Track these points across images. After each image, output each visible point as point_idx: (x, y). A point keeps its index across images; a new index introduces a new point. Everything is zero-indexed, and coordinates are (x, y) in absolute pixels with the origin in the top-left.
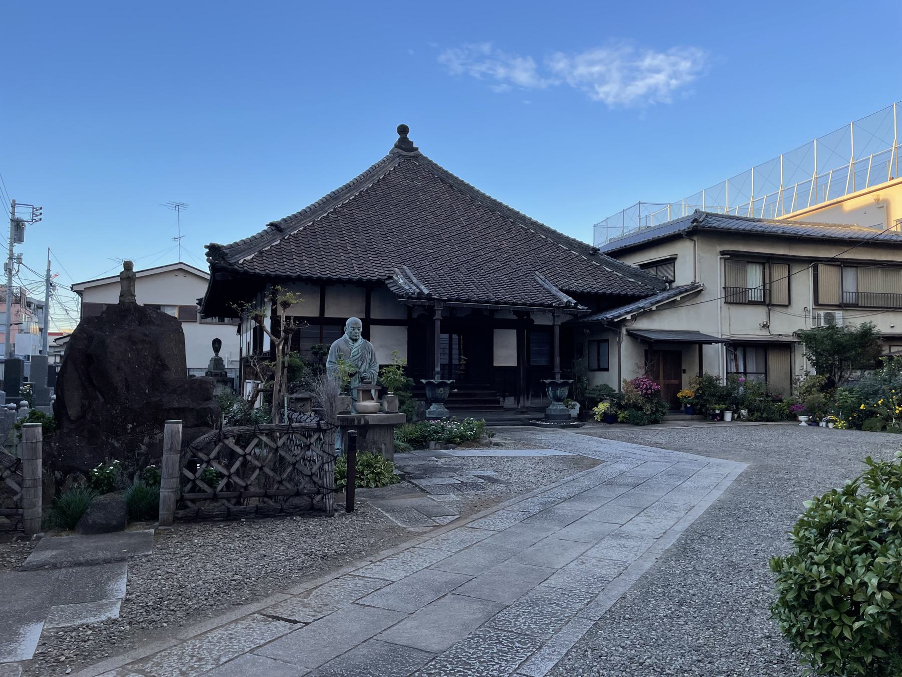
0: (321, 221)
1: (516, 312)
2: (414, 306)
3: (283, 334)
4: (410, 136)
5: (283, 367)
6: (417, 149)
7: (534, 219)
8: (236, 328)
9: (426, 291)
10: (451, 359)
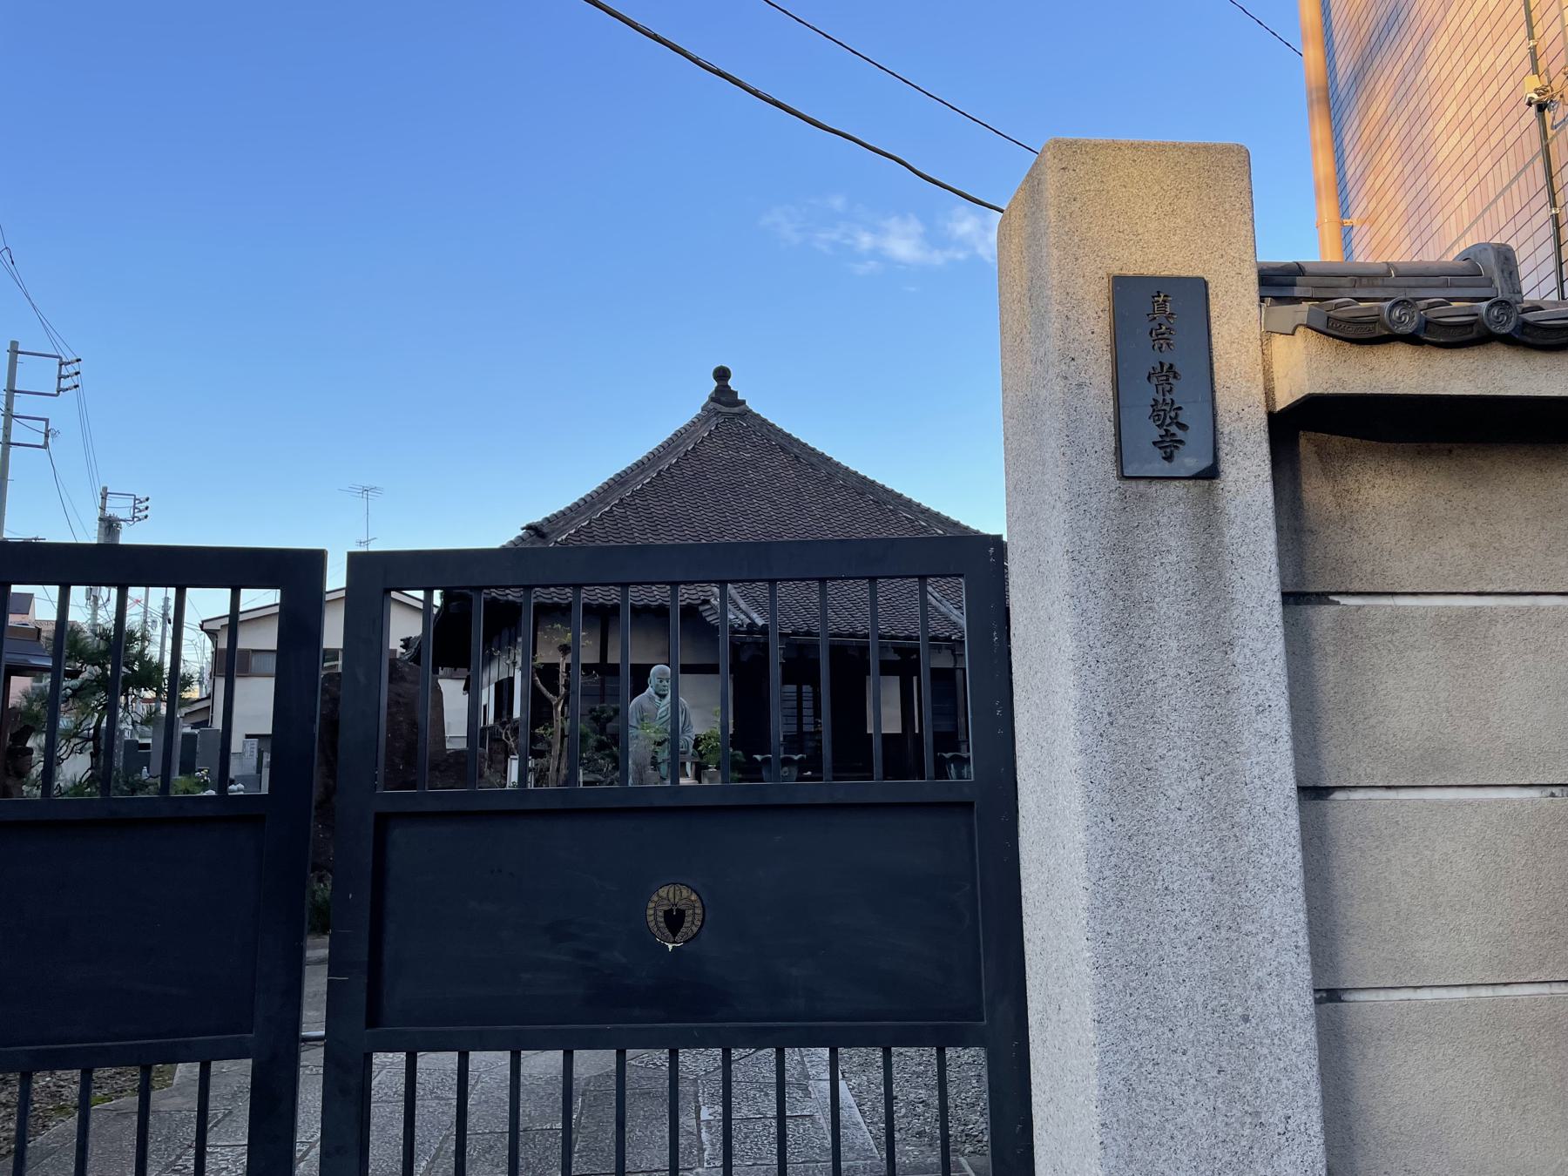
0: (600, 518)
1: (898, 650)
2: (743, 644)
3: (562, 690)
4: (732, 383)
5: (563, 736)
6: (743, 402)
7: (926, 504)
8: (463, 683)
9: (760, 622)
10: (800, 724)
